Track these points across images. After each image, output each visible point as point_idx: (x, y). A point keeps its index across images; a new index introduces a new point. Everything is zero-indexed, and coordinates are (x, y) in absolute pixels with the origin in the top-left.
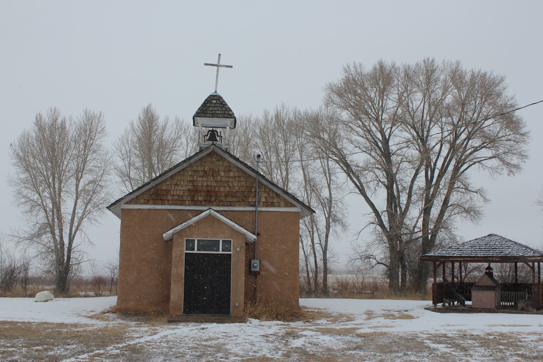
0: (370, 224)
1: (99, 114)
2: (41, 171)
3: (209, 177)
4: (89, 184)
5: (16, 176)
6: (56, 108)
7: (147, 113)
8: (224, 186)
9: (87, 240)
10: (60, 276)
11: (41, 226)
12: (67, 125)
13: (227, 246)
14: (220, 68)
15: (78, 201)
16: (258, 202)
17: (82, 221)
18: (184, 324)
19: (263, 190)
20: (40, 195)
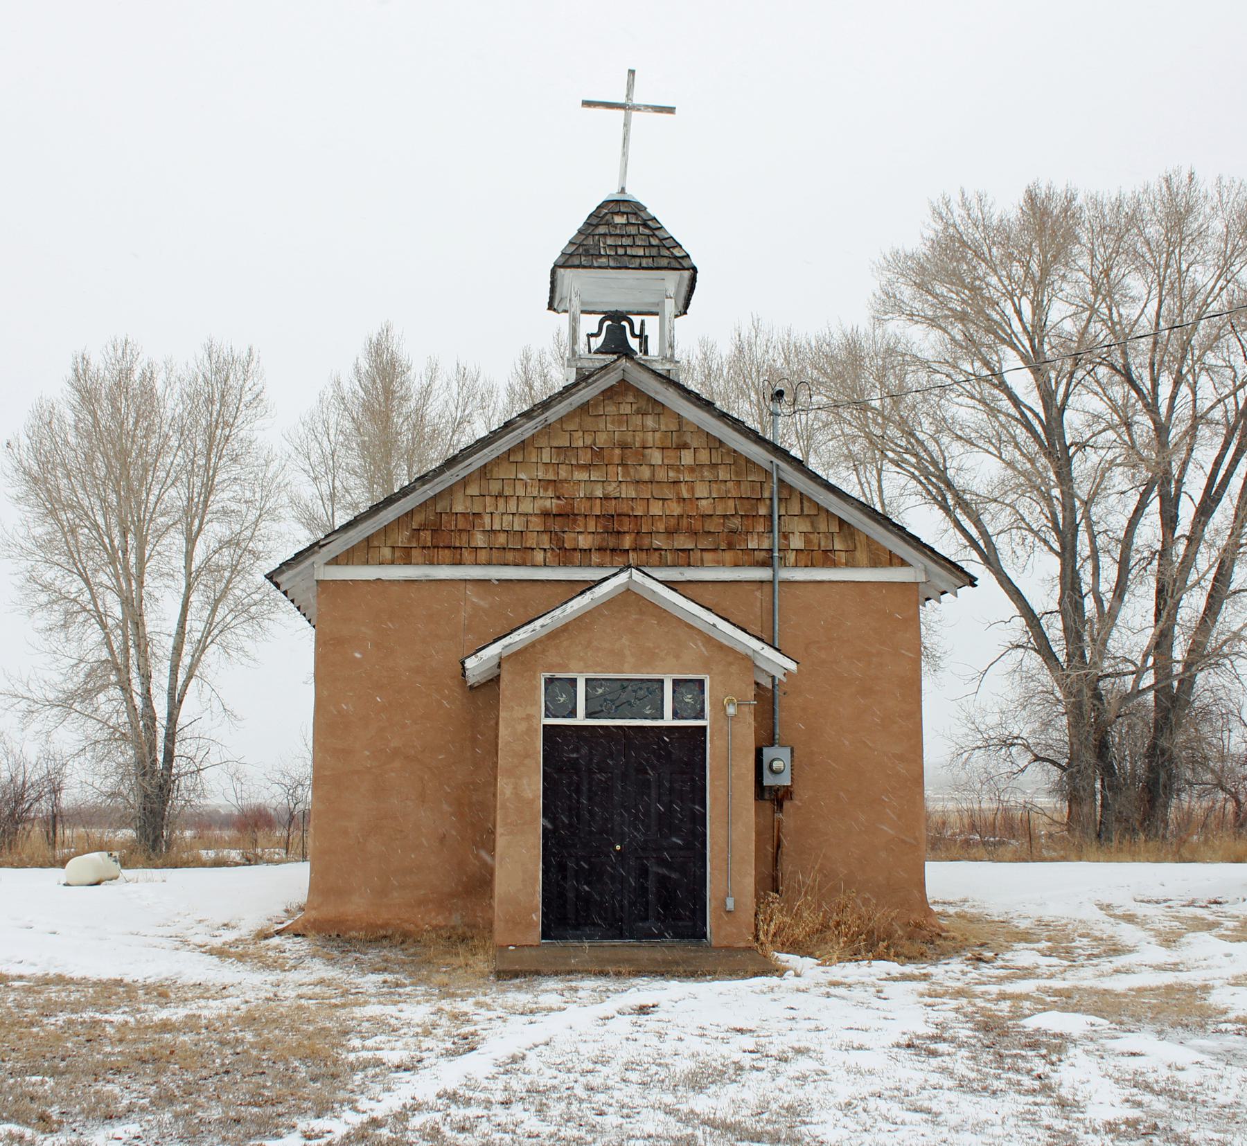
0: (1013, 648)
1: (245, 354)
2: (86, 514)
3: (610, 467)
4: (221, 548)
5: (22, 531)
6: (126, 341)
7: (378, 353)
8: (664, 499)
9: (216, 704)
10: (144, 809)
11: (93, 670)
12: (159, 386)
13: (688, 699)
14: (634, 114)
15: (191, 599)
16: (779, 550)
17: (203, 651)
18: (561, 986)
19: (795, 509)
20: (87, 581)
